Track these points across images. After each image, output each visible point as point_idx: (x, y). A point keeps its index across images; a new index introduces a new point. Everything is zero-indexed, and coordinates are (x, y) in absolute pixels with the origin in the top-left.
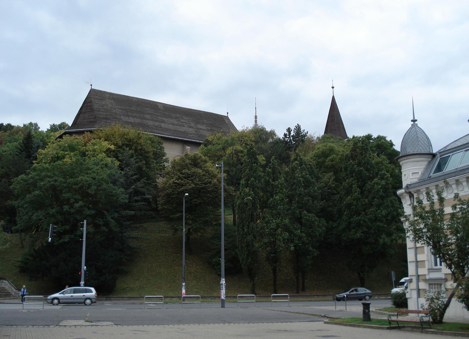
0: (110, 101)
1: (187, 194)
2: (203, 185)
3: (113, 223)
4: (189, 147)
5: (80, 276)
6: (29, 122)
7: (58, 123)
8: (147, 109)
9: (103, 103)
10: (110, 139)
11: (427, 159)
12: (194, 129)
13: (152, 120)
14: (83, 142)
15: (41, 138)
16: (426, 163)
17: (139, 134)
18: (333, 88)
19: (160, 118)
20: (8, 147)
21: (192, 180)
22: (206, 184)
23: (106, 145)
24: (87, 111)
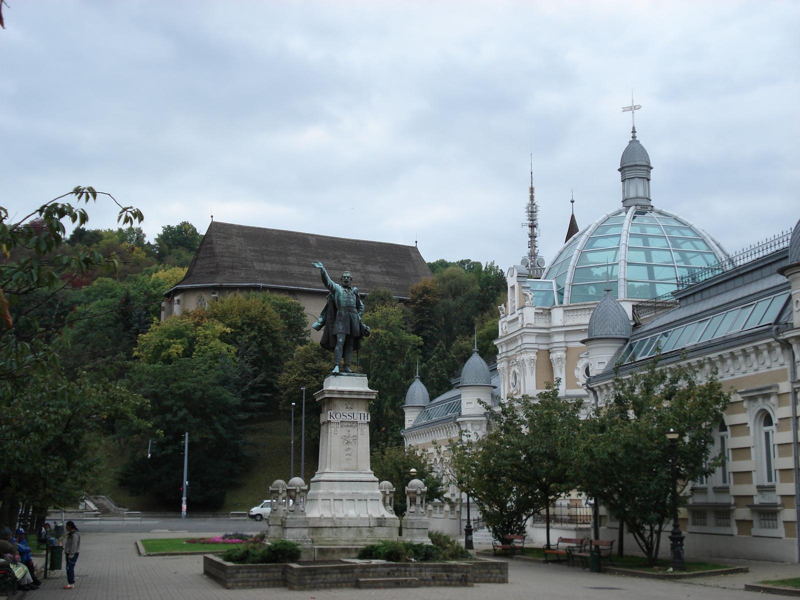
0: (239, 239)
3: (221, 430)
5: (182, 491)
8: (292, 247)
9: (229, 243)
13: (299, 265)
15: (146, 289)
16: (419, 413)
17: (264, 308)
18: (572, 202)
21: (317, 377)
23: (220, 327)
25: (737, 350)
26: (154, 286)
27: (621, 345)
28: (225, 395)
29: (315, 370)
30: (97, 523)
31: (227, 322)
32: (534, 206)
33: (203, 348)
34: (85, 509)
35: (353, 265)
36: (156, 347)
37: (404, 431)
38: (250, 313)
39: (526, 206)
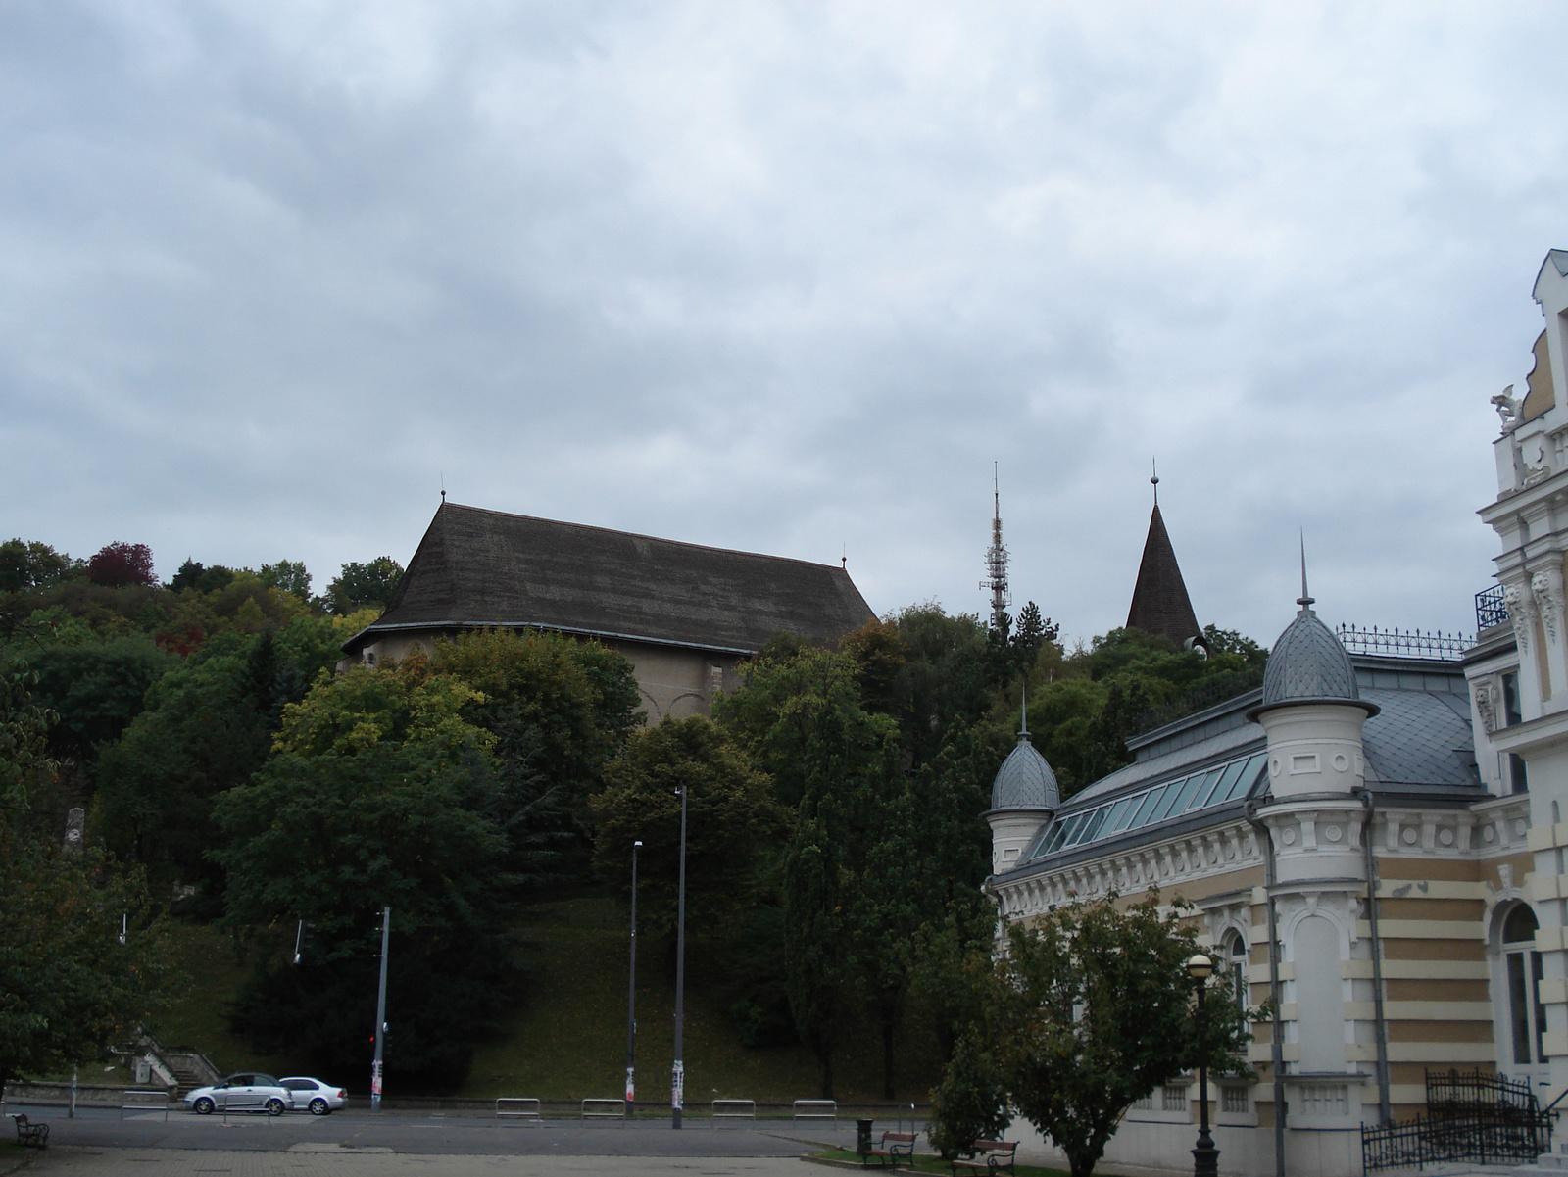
0: (496, 538)
1: (640, 843)
2: (707, 807)
4: (719, 670)
6: (279, 561)
7: (366, 559)
10: (477, 671)
11: (1037, 822)
12: (736, 613)
13: (615, 591)
14: (402, 683)
15: (306, 639)
16: (1034, 830)
17: (555, 655)
18: (1155, 482)
19: (637, 583)
20: (211, 669)
22: (714, 803)
23: (462, 690)
24: (429, 567)
25: (1043, 876)
26: (321, 634)
27: (1044, 822)
28: (474, 827)
29: (673, 778)
30: (159, 1117)
31: (478, 681)
32: (1001, 553)
33: (426, 731)
34: (150, 1083)
35: (722, 596)
36: (322, 728)
37: (996, 880)
38: (525, 665)
39: (986, 551)
